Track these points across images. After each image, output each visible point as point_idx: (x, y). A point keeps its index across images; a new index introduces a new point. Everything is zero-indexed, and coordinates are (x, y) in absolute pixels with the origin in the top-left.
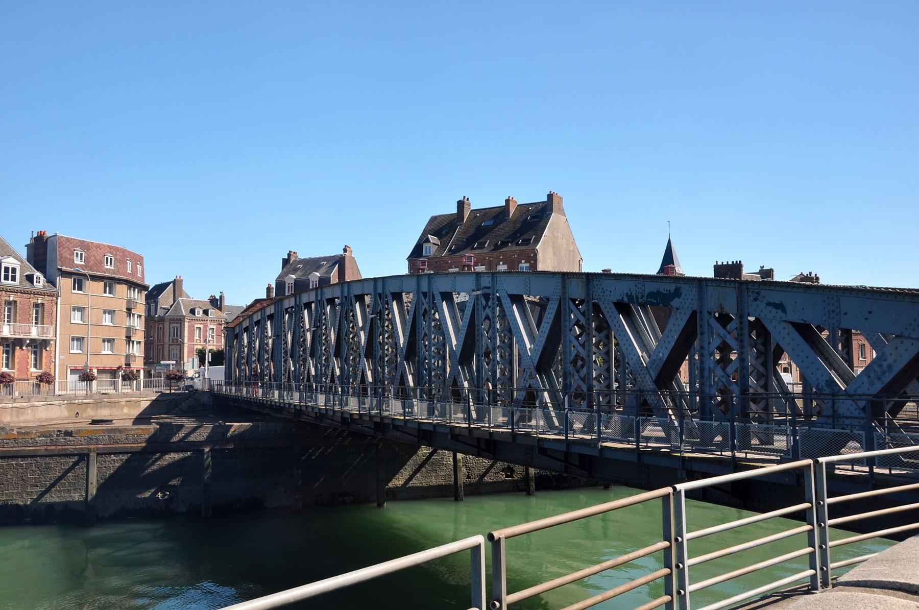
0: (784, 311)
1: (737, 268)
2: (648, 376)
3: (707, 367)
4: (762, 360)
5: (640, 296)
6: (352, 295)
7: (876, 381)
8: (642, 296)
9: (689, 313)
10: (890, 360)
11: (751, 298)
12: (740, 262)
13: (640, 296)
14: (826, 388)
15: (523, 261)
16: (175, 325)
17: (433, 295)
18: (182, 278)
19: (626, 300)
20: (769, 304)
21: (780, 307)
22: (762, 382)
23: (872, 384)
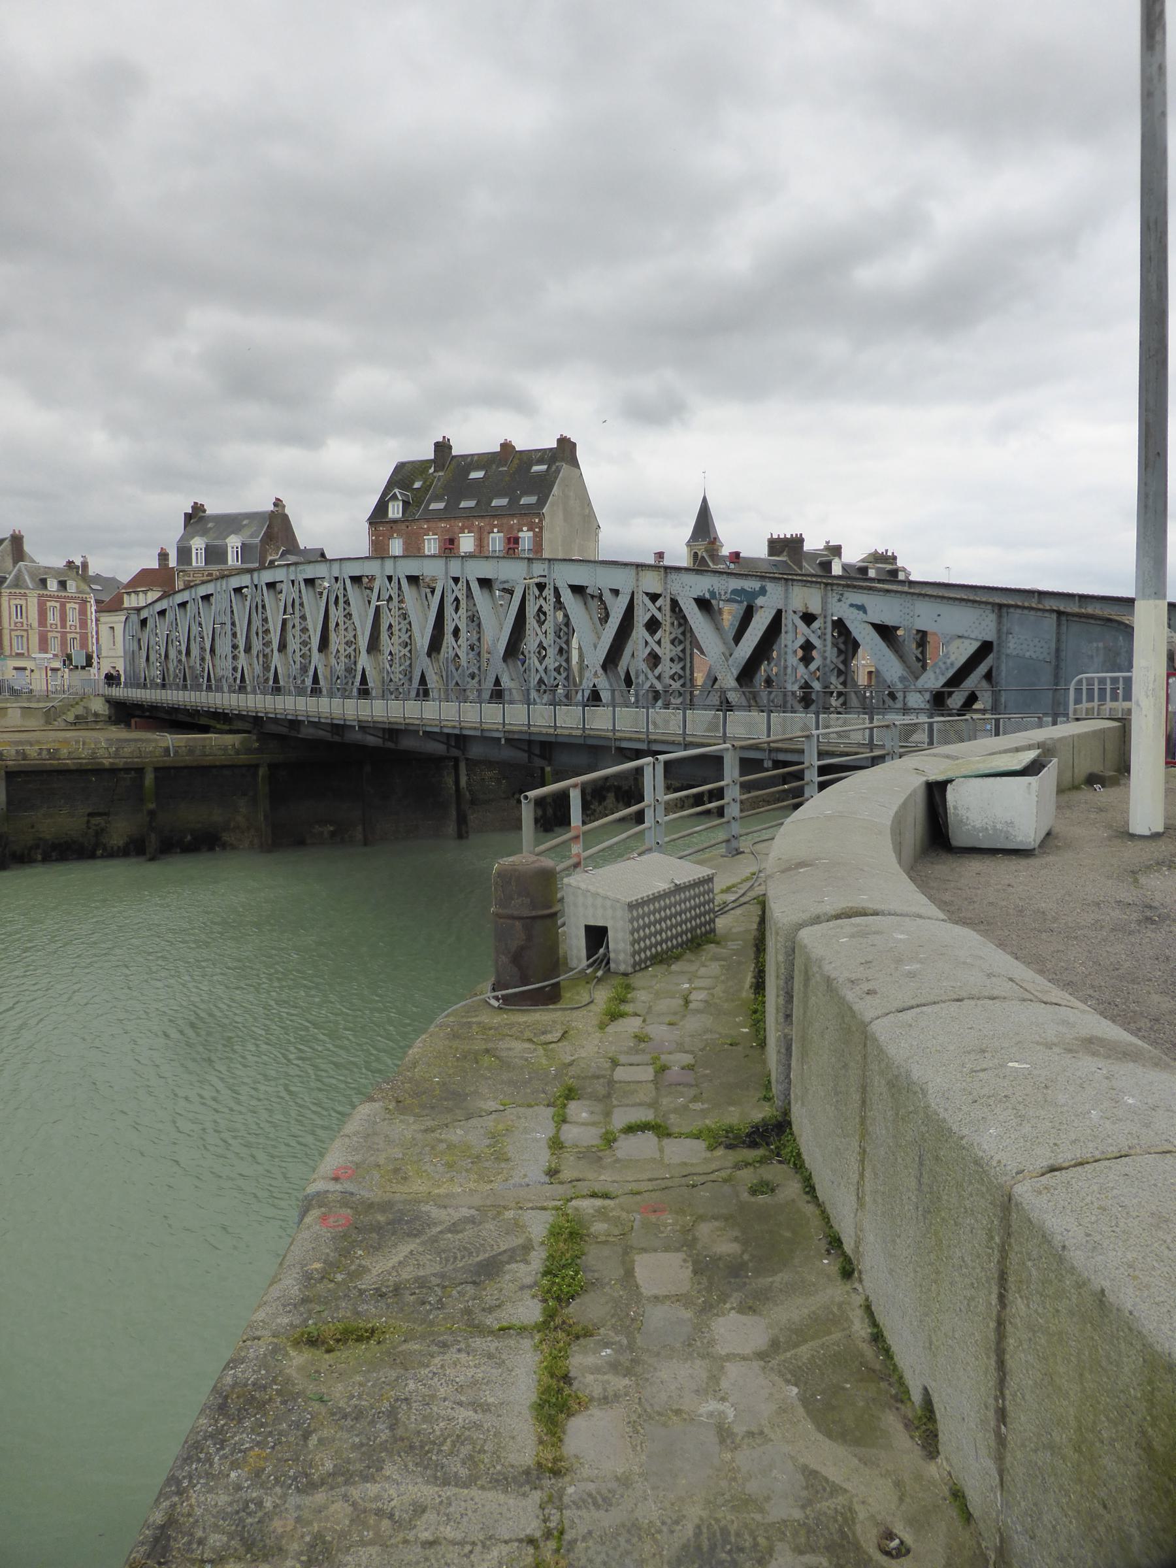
0: (865, 612)
1: (797, 542)
2: (729, 674)
3: (790, 665)
4: (842, 658)
5: (723, 593)
6: (346, 577)
7: (940, 677)
8: (726, 593)
9: (773, 612)
10: (953, 658)
11: (835, 599)
12: (801, 535)
13: (723, 593)
14: (898, 683)
15: (525, 529)
16: (18, 602)
17: (467, 581)
18: (22, 533)
19: (707, 596)
20: (852, 605)
21: (862, 608)
22: (842, 679)
23: (937, 679)
